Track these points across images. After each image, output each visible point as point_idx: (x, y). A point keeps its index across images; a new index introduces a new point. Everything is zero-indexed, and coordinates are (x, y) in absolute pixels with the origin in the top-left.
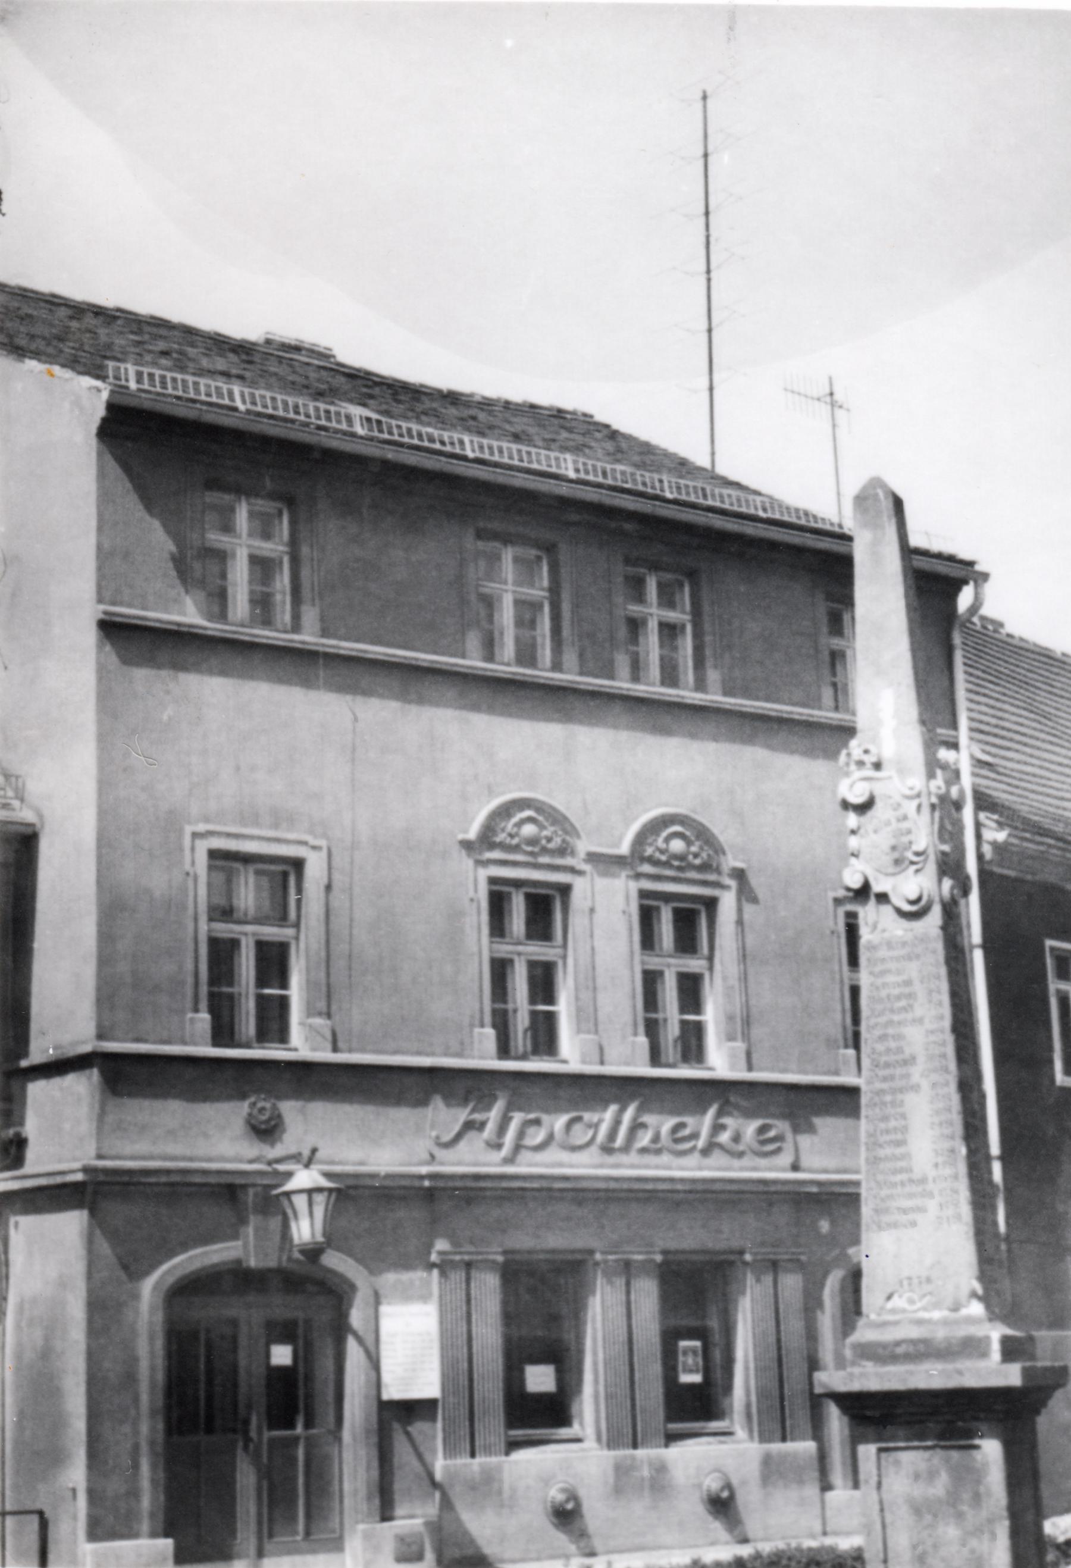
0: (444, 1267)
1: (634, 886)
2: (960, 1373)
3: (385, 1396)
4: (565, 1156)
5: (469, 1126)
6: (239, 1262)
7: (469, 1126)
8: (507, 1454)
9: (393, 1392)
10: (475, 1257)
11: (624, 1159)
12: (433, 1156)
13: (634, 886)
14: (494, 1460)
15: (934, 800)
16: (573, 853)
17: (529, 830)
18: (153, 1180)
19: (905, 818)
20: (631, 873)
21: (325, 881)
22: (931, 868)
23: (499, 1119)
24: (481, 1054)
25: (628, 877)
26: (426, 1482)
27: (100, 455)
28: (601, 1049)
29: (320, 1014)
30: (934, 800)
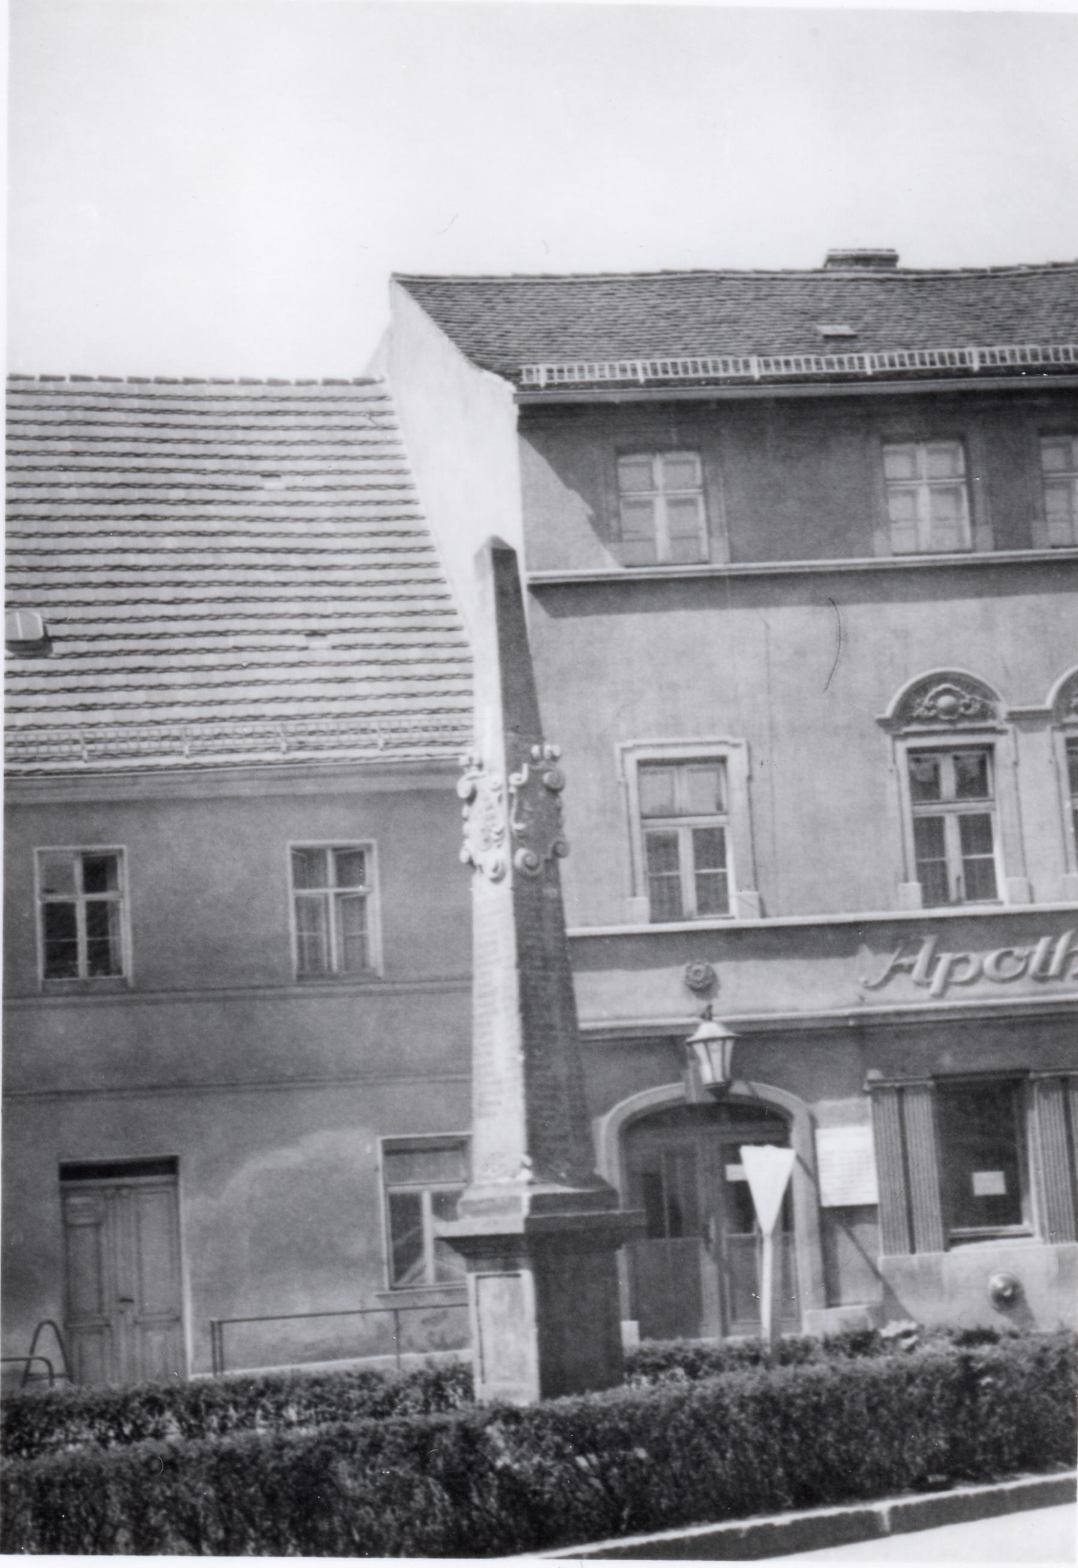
0: (877, 1092)
1: (1060, 737)
2: (496, 1223)
3: (826, 1203)
4: (997, 988)
5: (896, 969)
6: (682, 1098)
7: (896, 969)
8: (946, 1249)
9: (832, 1198)
10: (904, 1084)
11: (1058, 985)
12: (862, 999)
13: (1060, 737)
14: (933, 1255)
15: (513, 790)
16: (994, 716)
17: (945, 701)
18: (599, 1037)
19: (491, 807)
20: (1057, 725)
21: (746, 773)
22: (506, 844)
23: (926, 962)
24: (909, 903)
25: (1053, 729)
26: (871, 1274)
27: (521, 447)
28: (1031, 889)
29: (748, 887)
30: (513, 790)
